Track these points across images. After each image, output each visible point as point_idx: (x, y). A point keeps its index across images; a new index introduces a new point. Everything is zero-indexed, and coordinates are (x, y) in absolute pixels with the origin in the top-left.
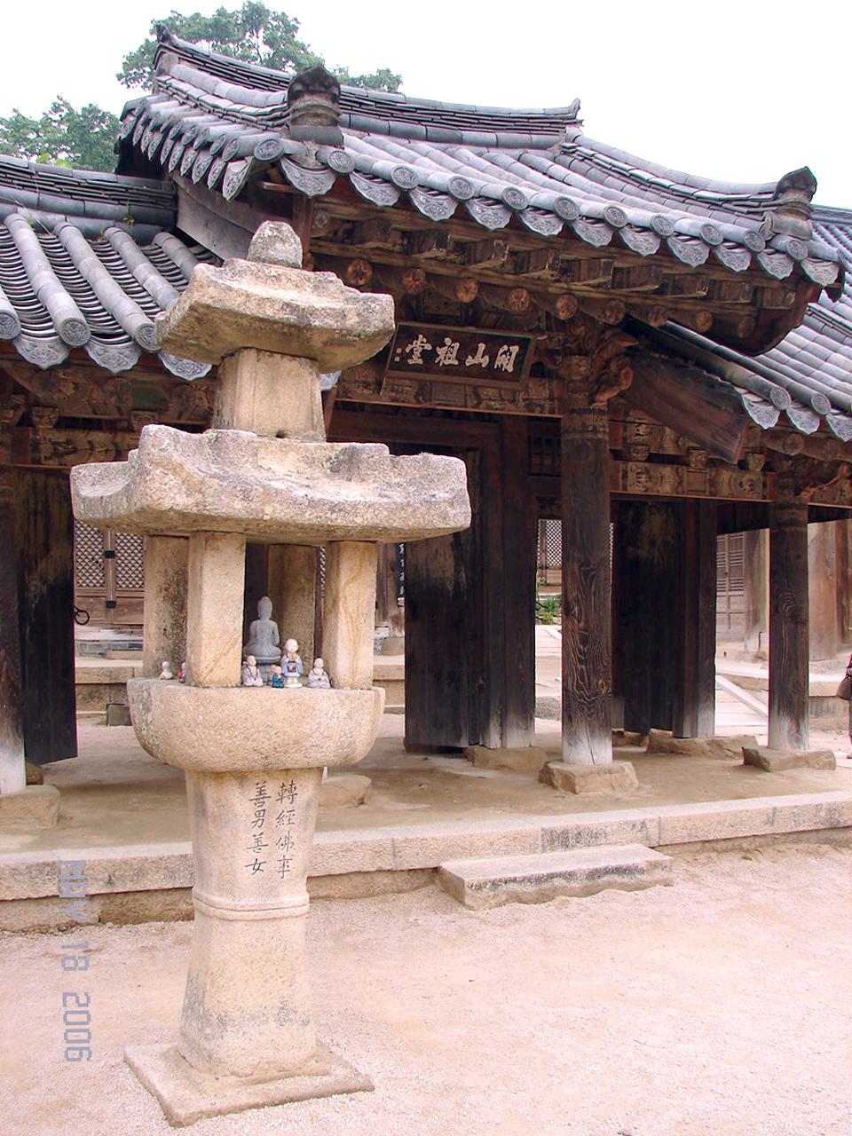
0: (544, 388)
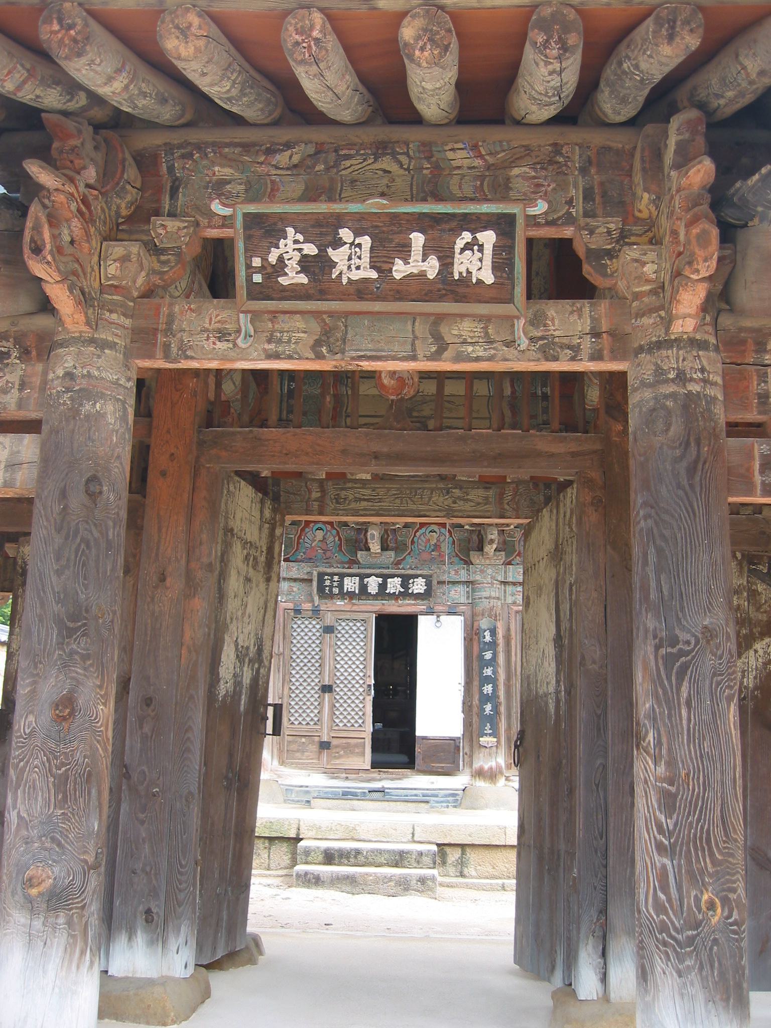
0: (580, 317)
